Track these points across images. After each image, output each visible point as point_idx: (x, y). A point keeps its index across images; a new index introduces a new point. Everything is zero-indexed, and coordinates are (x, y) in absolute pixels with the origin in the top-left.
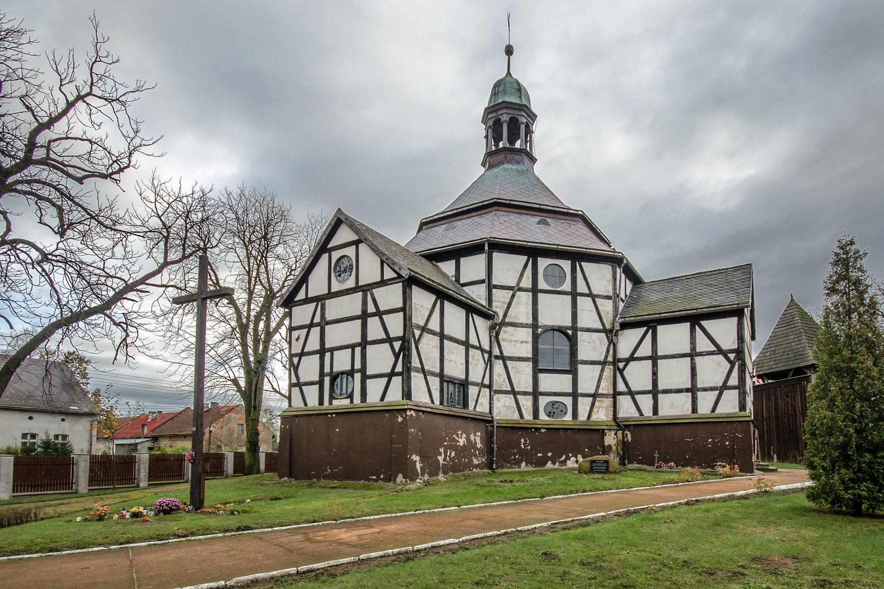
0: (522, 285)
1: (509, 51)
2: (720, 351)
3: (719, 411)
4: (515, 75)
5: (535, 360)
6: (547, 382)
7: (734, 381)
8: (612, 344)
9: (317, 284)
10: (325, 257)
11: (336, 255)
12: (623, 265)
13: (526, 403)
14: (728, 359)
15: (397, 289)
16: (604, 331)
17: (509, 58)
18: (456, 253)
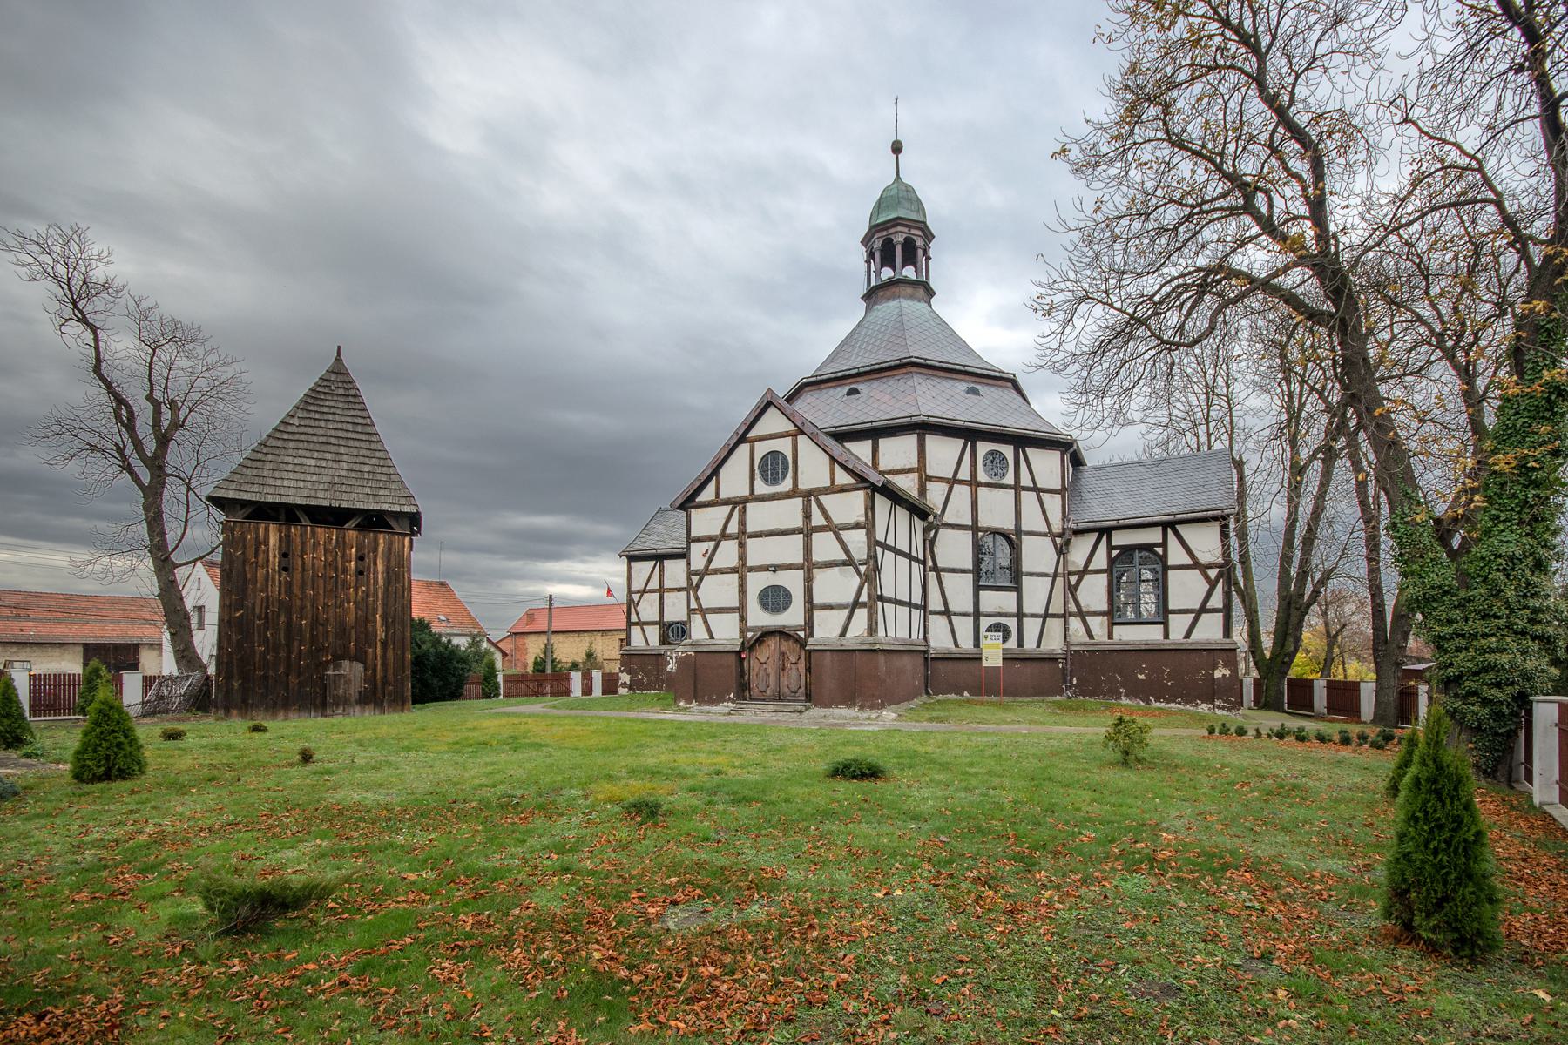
0: (960, 477)
1: (897, 148)
2: (1196, 565)
3: (1195, 636)
4: (905, 179)
5: (977, 571)
6: (991, 601)
7: (1217, 601)
8: (1062, 552)
9: (734, 483)
10: (744, 449)
11: (762, 449)
12: (1072, 450)
13: (964, 627)
14: (1207, 577)
15: (859, 498)
16: (1050, 534)
17: (897, 158)
18: (875, 433)
